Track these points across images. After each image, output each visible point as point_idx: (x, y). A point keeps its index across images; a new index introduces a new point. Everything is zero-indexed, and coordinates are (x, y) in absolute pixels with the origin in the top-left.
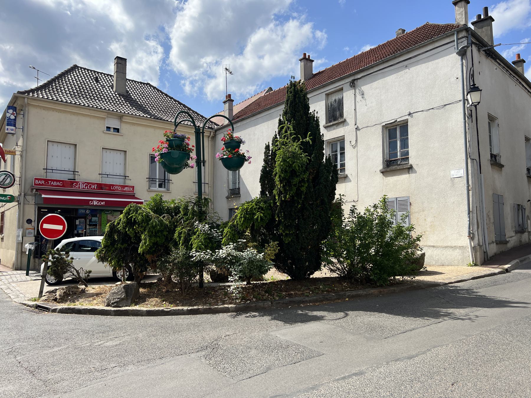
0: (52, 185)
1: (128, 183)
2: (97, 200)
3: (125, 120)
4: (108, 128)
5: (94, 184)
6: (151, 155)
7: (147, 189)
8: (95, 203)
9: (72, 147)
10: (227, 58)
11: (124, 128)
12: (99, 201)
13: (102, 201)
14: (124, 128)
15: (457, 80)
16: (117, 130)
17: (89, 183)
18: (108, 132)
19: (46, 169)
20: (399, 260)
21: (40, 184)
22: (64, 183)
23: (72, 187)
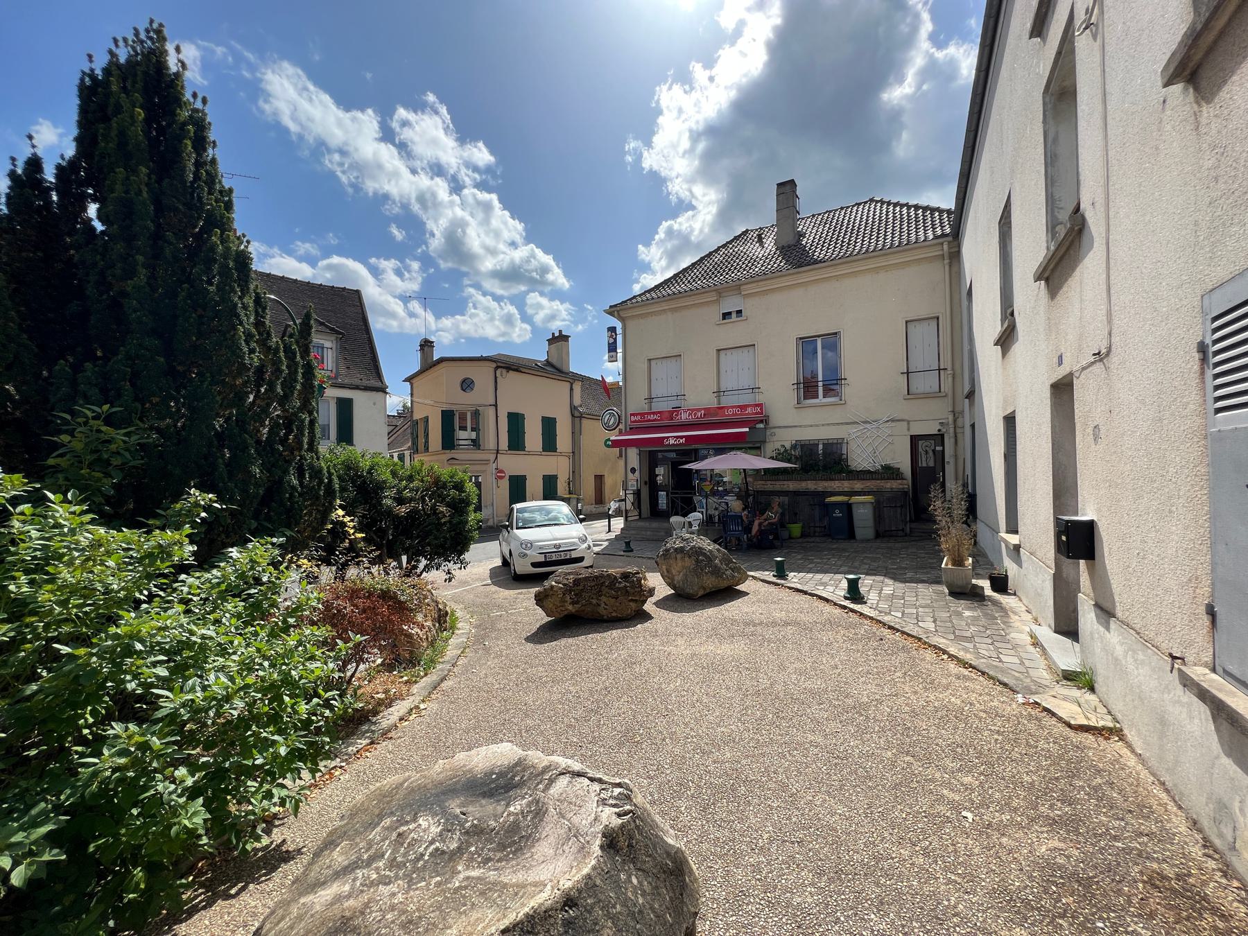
0: (649, 420)
1: (760, 399)
2: (674, 437)
3: (746, 293)
4: (726, 315)
5: (699, 410)
6: (801, 339)
7: (904, 395)
8: (672, 442)
9: (911, 326)
10: (897, 86)
11: (748, 306)
12: (677, 437)
13: (681, 437)
14: (748, 306)
15: (752, 41)
16: (739, 312)
17: (692, 410)
18: (739, 319)
19: (939, 370)
20: (381, 505)
21: (635, 421)
22: (708, 411)
23: (672, 419)
